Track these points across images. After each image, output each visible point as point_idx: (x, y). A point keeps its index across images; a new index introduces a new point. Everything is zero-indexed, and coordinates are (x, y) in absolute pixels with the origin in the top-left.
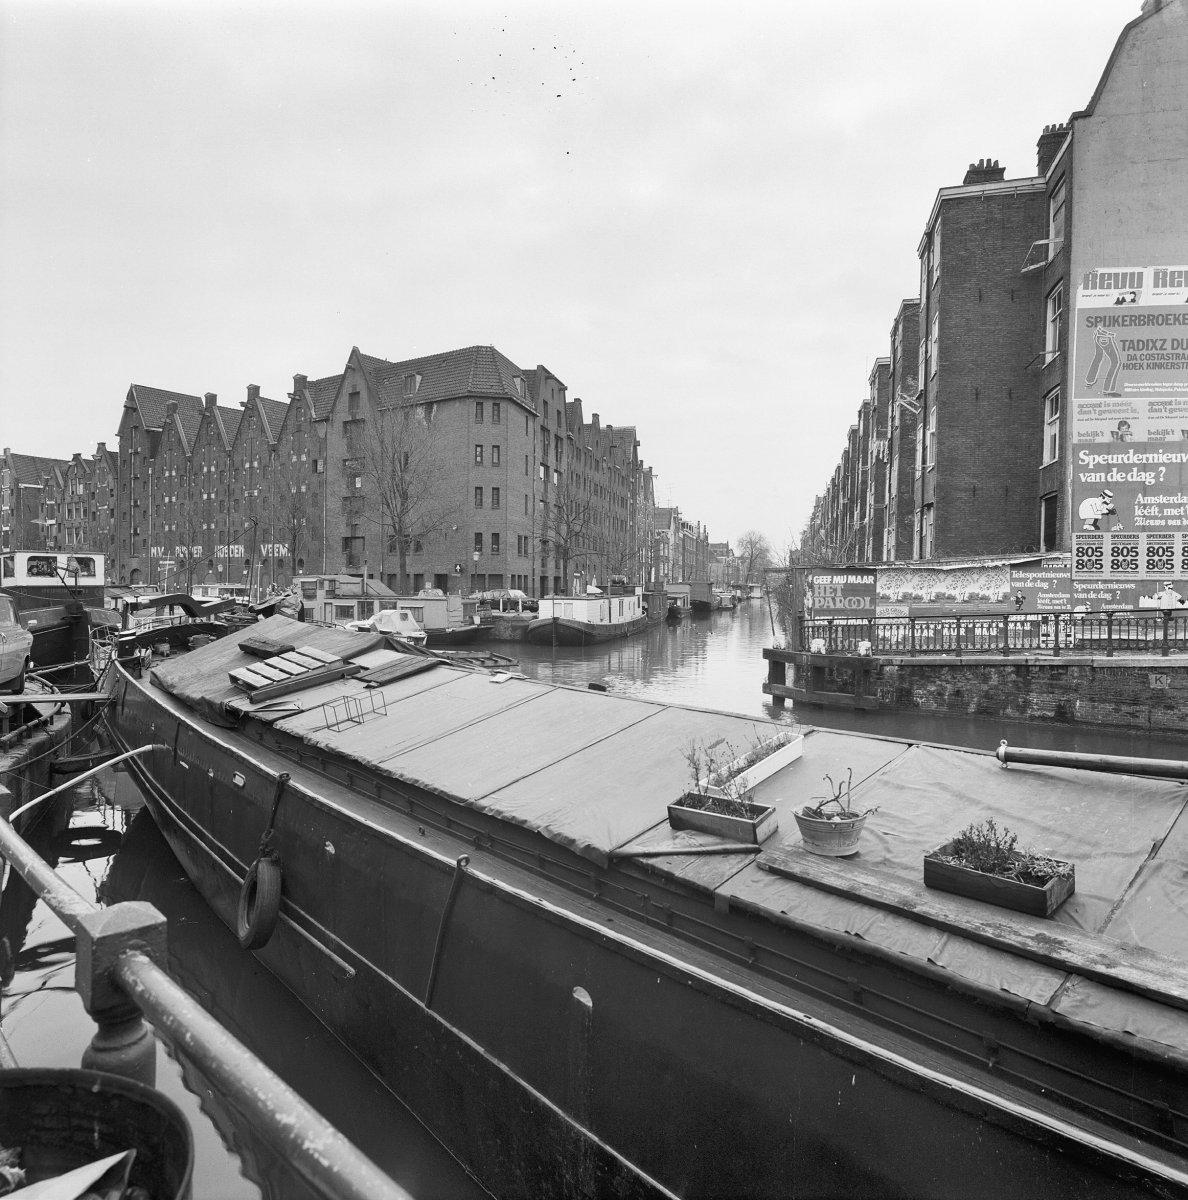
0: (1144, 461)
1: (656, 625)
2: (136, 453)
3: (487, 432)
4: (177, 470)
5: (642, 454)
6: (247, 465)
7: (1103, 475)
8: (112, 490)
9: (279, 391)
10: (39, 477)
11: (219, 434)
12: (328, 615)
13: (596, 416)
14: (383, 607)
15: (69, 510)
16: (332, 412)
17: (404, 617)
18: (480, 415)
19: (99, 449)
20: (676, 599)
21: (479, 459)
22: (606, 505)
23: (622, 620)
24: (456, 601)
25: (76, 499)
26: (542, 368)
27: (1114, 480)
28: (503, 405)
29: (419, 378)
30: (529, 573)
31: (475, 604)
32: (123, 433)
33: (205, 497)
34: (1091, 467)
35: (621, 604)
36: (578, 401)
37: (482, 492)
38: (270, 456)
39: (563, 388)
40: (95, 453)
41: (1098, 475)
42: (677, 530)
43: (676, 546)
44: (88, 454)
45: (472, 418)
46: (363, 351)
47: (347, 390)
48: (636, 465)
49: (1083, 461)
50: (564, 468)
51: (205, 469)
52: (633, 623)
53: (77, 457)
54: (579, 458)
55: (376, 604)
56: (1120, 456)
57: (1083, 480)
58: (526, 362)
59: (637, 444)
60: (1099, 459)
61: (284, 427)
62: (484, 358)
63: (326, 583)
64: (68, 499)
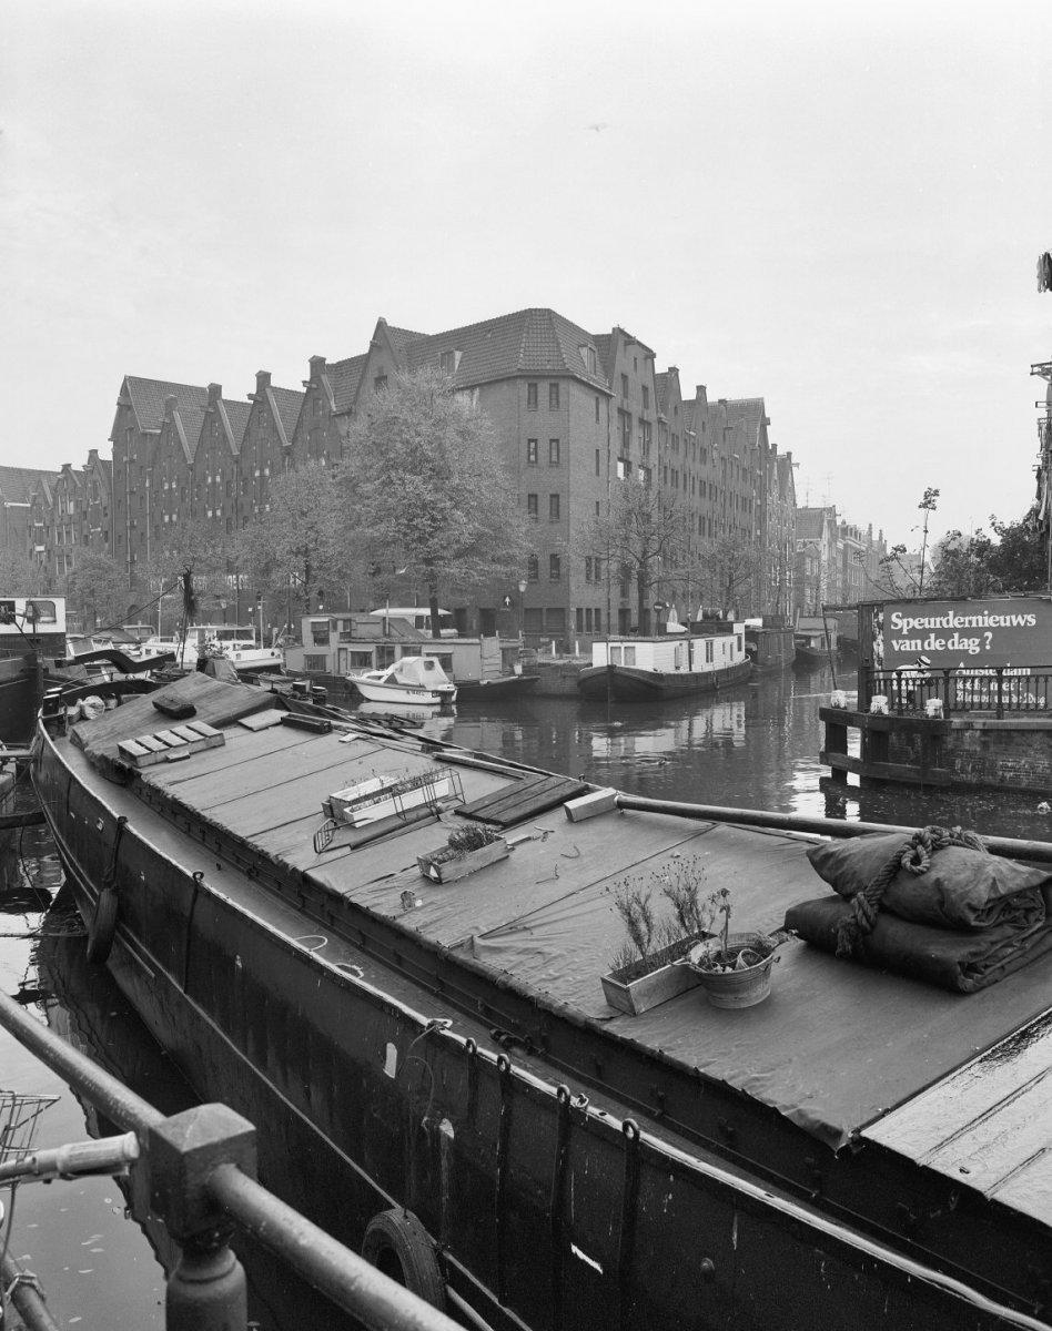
0: (967, 625)
1: (772, 674)
2: (132, 461)
3: (542, 423)
4: (178, 481)
5: (773, 436)
6: (257, 474)
7: (919, 642)
8: (105, 508)
9: (292, 377)
10: (26, 493)
11: (225, 436)
12: (343, 663)
13: (701, 389)
14: (406, 652)
15: (59, 534)
16: (355, 403)
17: (430, 666)
18: (533, 400)
19: (90, 457)
20: (808, 638)
21: (532, 457)
22: (718, 508)
23: (708, 668)
24: (493, 645)
25: (66, 520)
26: (619, 332)
27: (932, 648)
28: (563, 385)
29: (458, 355)
30: (602, 605)
31: (517, 648)
32: (116, 437)
33: (210, 514)
34: (905, 632)
35: (709, 646)
36: (674, 370)
37: (536, 500)
38: (284, 461)
39: (650, 355)
40: (86, 463)
41: (913, 642)
42: (833, 538)
43: (832, 561)
44: (79, 463)
45: (524, 403)
46: (390, 323)
47: (372, 374)
48: (767, 452)
49: (896, 625)
50: (653, 460)
51: (210, 480)
52: (726, 672)
53: (66, 467)
54: (675, 448)
55: (398, 650)
56: (938, 620)
57: (897, 648)
58: (596, 324)
59: (766, 422)
60: (915, 623)
61: (299, 425)
62: (539, 324)
63: (340, 624)
64: (58, 521)
